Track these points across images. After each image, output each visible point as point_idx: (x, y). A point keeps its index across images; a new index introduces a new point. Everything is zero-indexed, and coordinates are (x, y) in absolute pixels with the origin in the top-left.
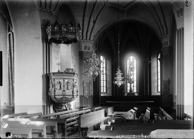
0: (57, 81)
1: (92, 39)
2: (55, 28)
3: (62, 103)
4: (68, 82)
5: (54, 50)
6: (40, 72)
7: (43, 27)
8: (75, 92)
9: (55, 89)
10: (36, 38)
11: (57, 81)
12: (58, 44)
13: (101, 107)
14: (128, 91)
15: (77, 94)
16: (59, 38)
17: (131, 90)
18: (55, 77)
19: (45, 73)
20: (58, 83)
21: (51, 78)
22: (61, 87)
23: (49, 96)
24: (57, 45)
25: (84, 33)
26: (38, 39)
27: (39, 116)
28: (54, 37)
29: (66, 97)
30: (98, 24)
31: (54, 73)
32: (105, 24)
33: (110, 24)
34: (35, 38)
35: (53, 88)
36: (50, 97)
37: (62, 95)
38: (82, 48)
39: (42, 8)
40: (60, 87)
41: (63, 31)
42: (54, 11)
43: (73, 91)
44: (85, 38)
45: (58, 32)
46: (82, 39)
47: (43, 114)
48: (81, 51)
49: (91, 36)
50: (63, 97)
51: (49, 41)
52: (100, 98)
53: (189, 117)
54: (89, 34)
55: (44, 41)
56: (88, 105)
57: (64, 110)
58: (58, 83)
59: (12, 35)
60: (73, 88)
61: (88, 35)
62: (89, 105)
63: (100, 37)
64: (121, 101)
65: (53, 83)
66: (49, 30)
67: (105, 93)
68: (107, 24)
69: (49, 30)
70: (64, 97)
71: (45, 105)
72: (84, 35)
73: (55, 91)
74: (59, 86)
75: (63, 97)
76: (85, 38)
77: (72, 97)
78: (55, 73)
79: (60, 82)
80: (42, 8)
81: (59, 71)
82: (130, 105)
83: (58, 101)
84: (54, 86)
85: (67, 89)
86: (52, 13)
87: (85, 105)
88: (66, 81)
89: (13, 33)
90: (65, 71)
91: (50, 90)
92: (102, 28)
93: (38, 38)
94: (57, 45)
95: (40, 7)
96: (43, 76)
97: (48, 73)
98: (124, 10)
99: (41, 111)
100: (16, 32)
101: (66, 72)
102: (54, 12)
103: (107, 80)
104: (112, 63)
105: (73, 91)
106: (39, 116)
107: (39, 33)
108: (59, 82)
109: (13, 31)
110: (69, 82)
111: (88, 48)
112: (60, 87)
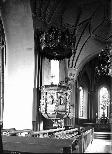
0: (50, 95)
1: (76, 67)
2: (50, 35)
3: (53, 119)
4: (61, 97)
5: (46, 69)
6: (31, 84)
7: (37, 37)
8: (68, 108)
9: (46, 104)
10: (29, 49)
11: (50, 95)
12: (50, 60)
13: (83, 127)
14: (101, 115)
15: (69, 111)
16: (53, 47)
17: (104, 115)
18: (47, 91)
19: (37, 87)
20: (50, 97)
21: (43, 92)
22: (54, 102)
23: (39, 112)
24: (49, 61)
25: (70, 61)
26: (31, 50)
27: (28, 133)
28: (48, 46)
29: (58, 112)
30: (82, 54)
31: (46, 86)
32: (87, 55)
33: (93, 55)
34: (28, 49)
35: (45, 103)
36: (41, 113)
37: (55, 110)
38: (68, 75)
39: (37, 14)
40: (53, 101)
41: (59, 39)
42: (48, 22)
43: (66, 107)
44: (70, 66)
45: (53, 40)
46: (69, 67)
47: (32, 131)
48: (66, 77)
49: (76, 65)
50: (56, 112)
51: (43, 55)
52: (78, 120)
53: (3, 128)
54: (74, 62)
55: (37, 52)
56: (71, 125)
57: (56, 128)
58: (50, 97)
59: (4, 49)
60: (66, 103)
61: (73, 64)
62: (72, 125)
63: (81, 71)
64: (91, 123)
65: (45, 98)
66: (43, 37)
67: (81, 116)
68: (91, 55)
69: (43, 37)
70: (56, 113)
71: (35, 121)
72: (70, 63)
73: (46, 106)
74: (51, 100)
75: (56, 112)
76: (70, 66)
77: (65, 113)
78: (48, 86)
79: (52, 97)
80: (37, 14)
81: (52, 84)
82: (102, 127)
83: (49, 118)
84: (46, 101)
85: (61, 104)
86: (46, 24)
87: (69, 125)
88: (59, 95)
89: (5, 46)
90: (59, 84)
91: (42, 105)
92: (86, 58)
93: (31, 49)
94: (49, 61)
95: (34, 15)
96: (34, 89)
97: (39, 87)
98: (106, 42)
99: (30, 127)
100: (9, 49)
101: (60, 84)
102: (48, 23)
103: (84, 106)
104: (89, 92)
105: (66, 107)
106: (28, 133)
107: (32, 44)
108: (51, 96)
109: (6, 45)
110: (62, 97)
111: (73, 76)
112: (53, 101)
